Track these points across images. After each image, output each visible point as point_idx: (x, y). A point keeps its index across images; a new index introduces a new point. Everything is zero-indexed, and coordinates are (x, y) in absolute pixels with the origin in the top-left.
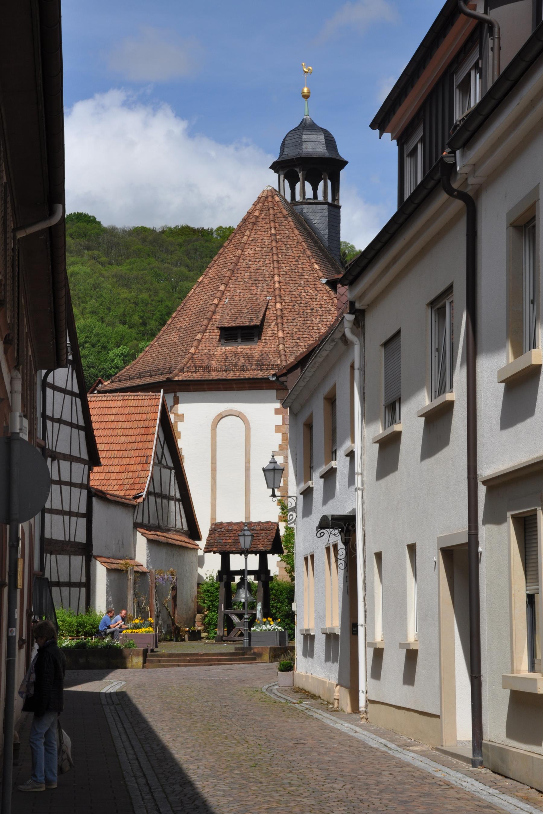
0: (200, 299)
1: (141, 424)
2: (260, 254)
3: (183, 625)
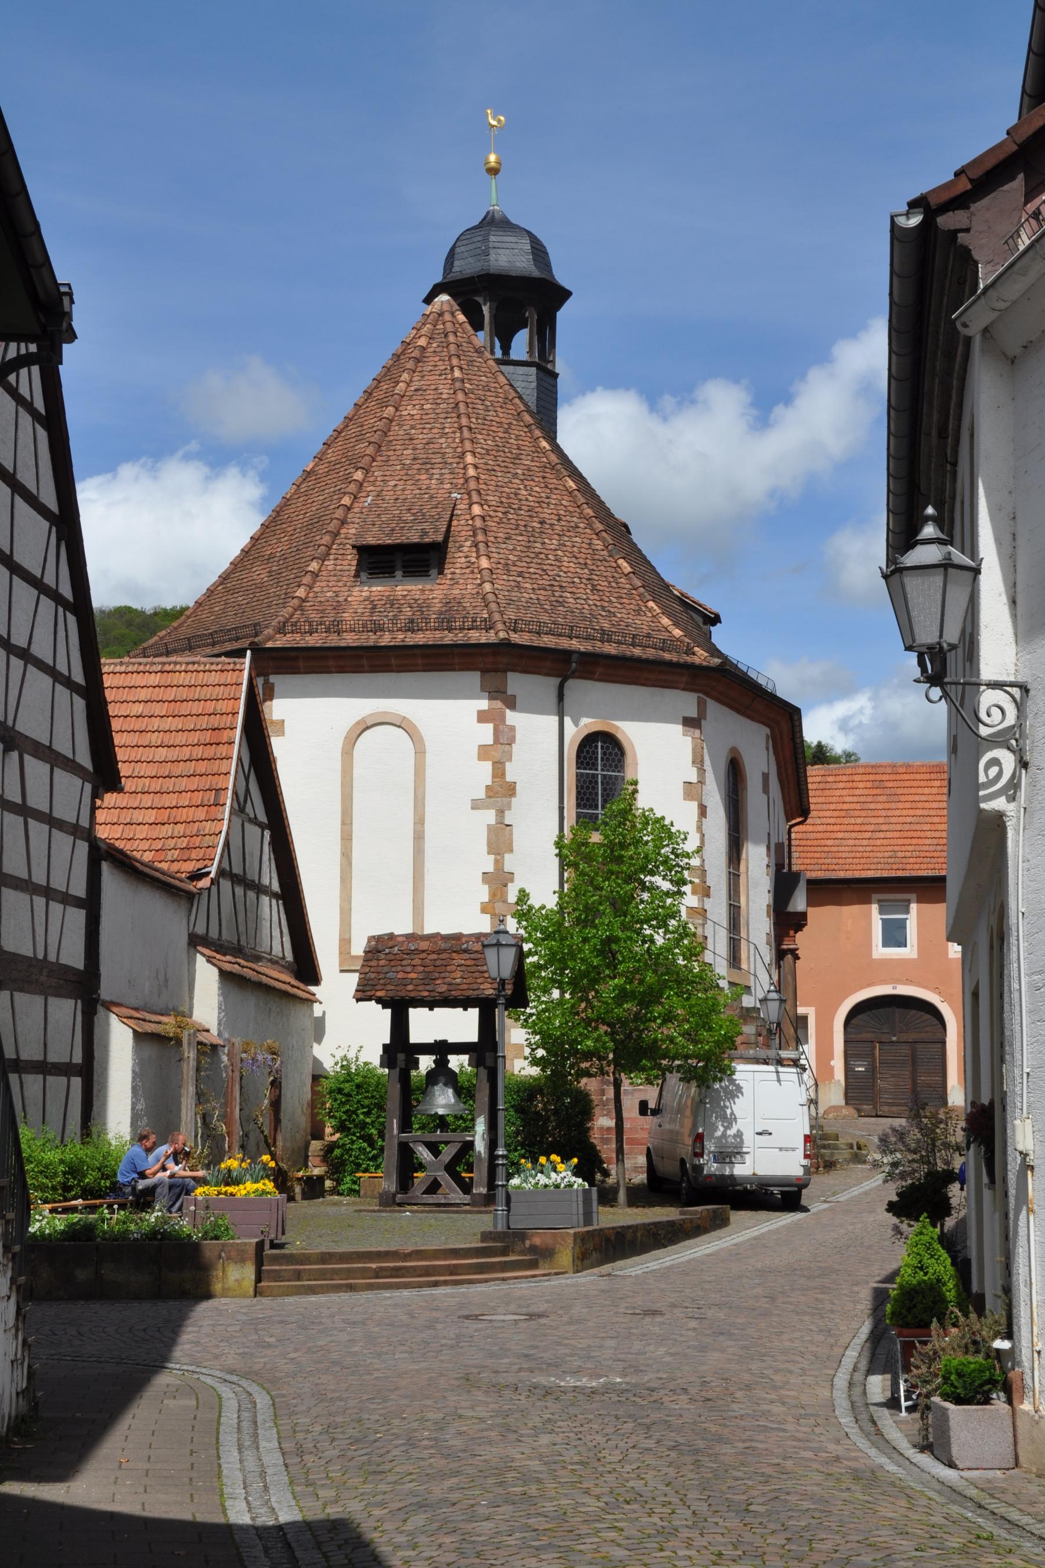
0: (310, 501)
1: (203, 722)
2: (432, 416)
3: (294, 1165)
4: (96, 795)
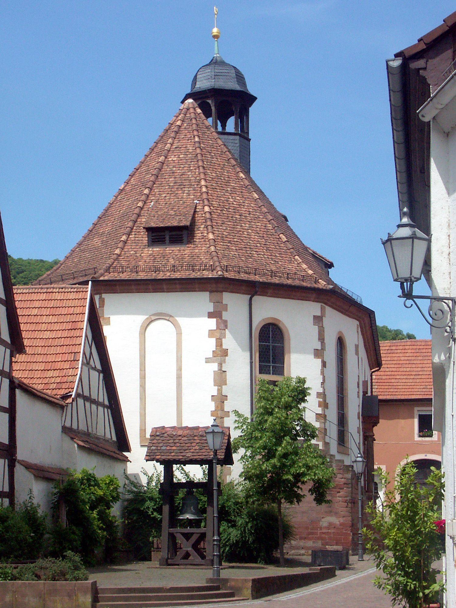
2: (184, 161)
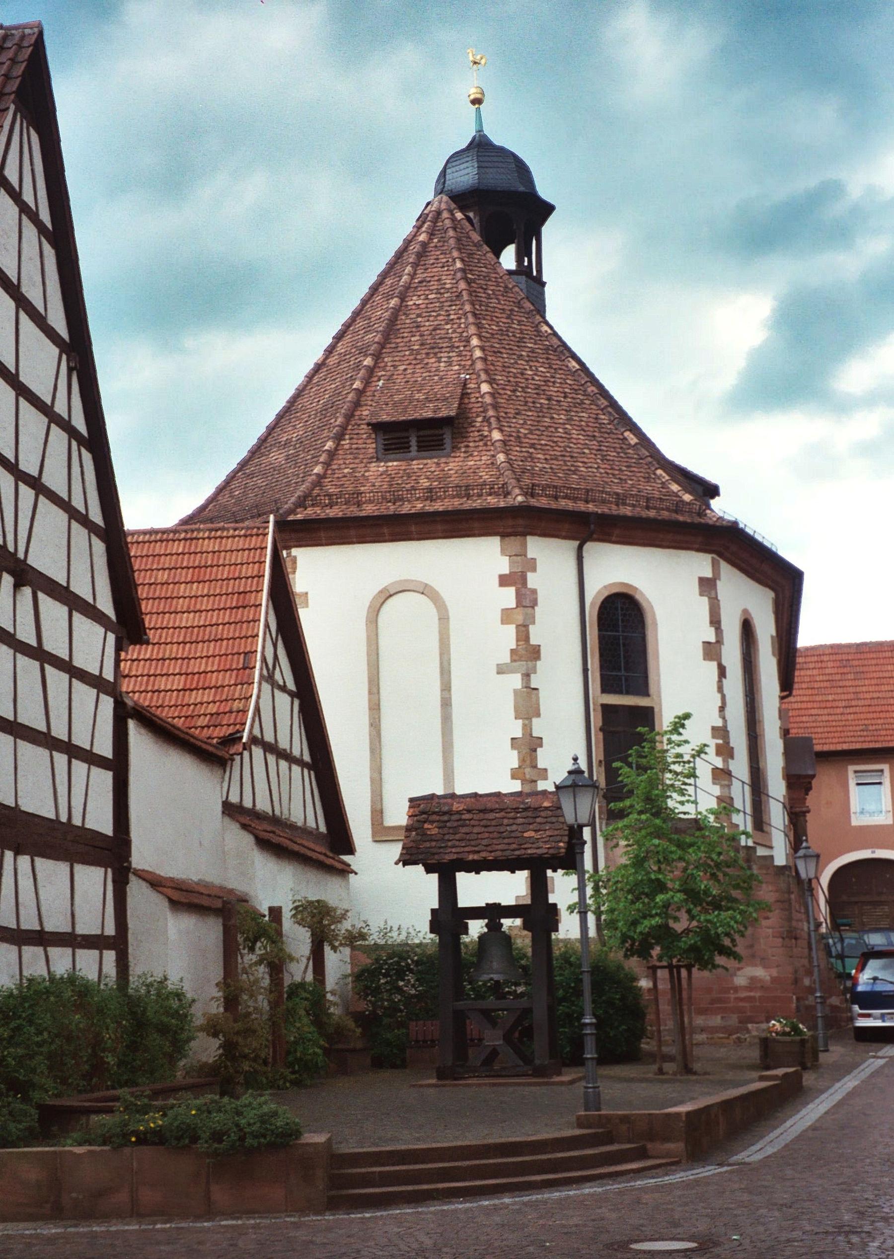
1: (231, 586)
2: (437, 305)
4: (119, 648)
